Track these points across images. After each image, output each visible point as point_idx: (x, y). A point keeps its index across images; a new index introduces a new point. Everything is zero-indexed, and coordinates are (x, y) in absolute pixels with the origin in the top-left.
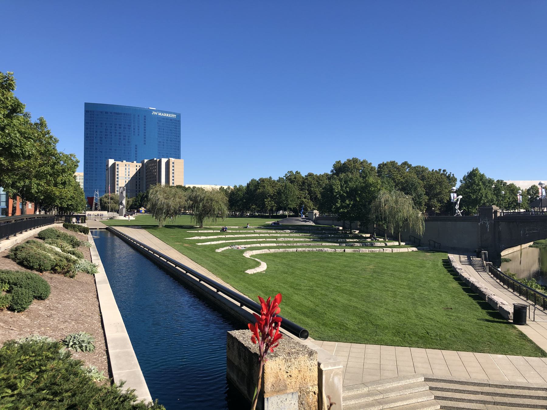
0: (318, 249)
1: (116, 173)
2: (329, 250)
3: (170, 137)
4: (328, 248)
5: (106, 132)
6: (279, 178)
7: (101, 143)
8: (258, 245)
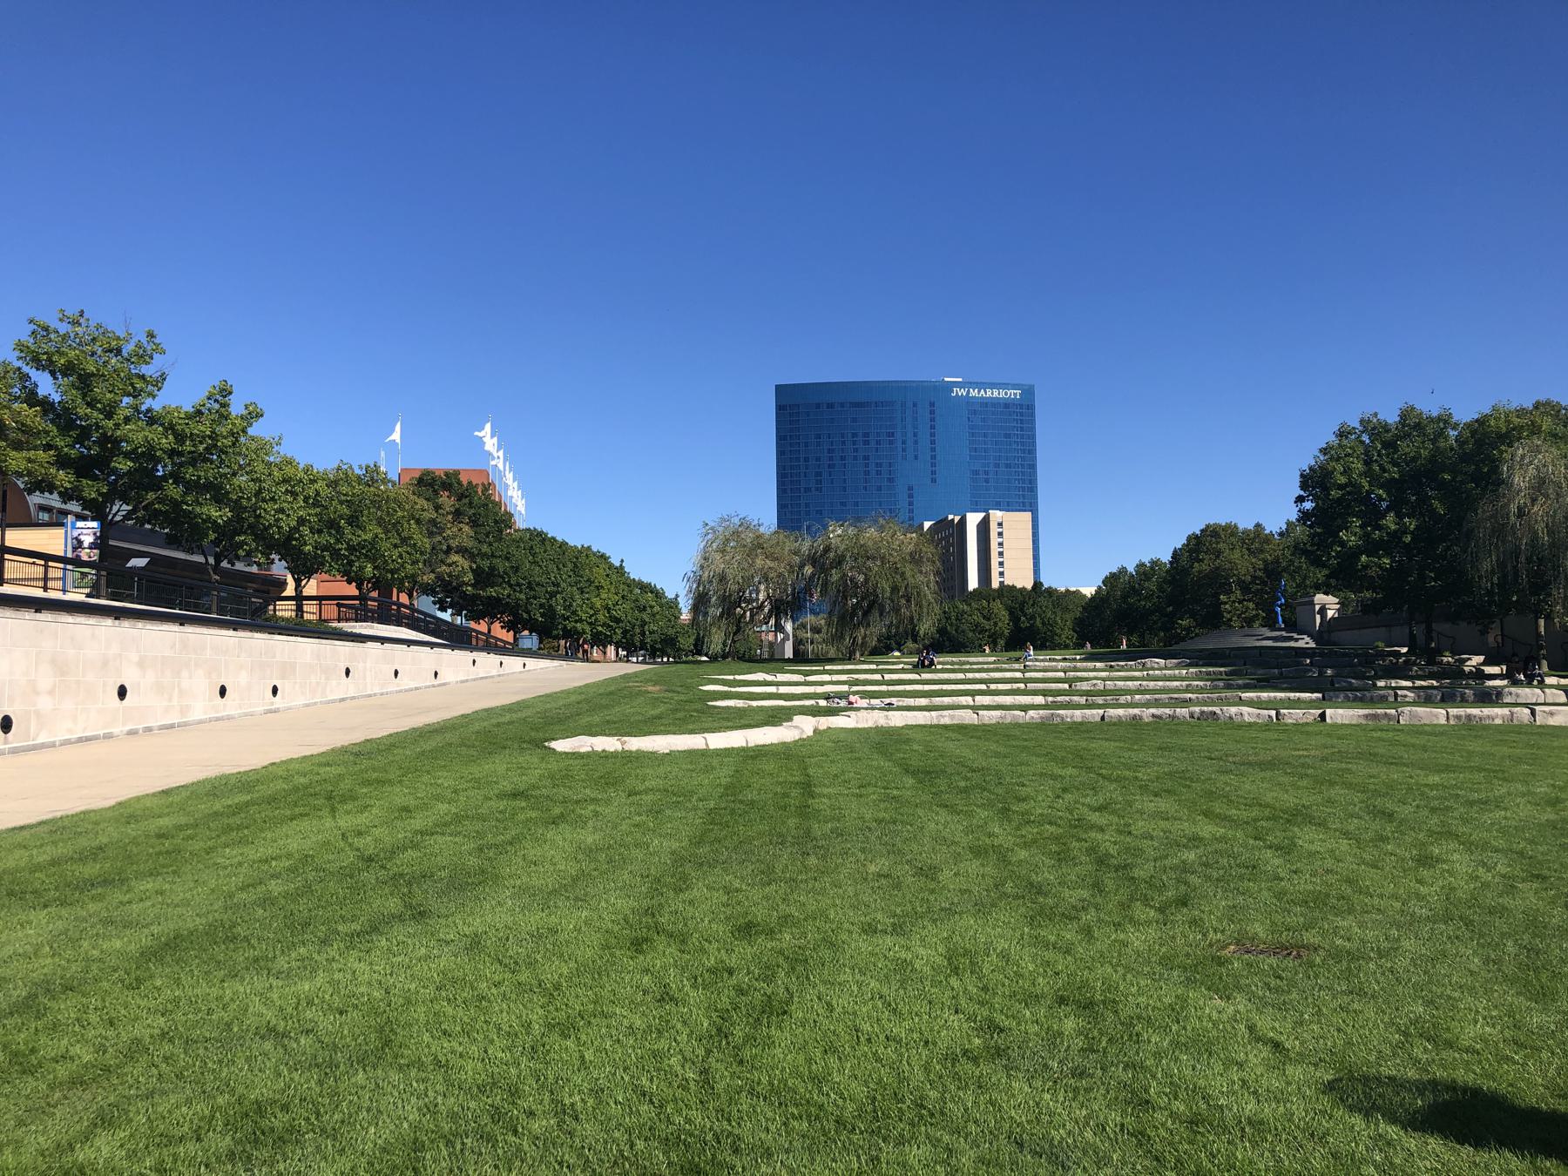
0: (1197, 709)
5: (831, 459)
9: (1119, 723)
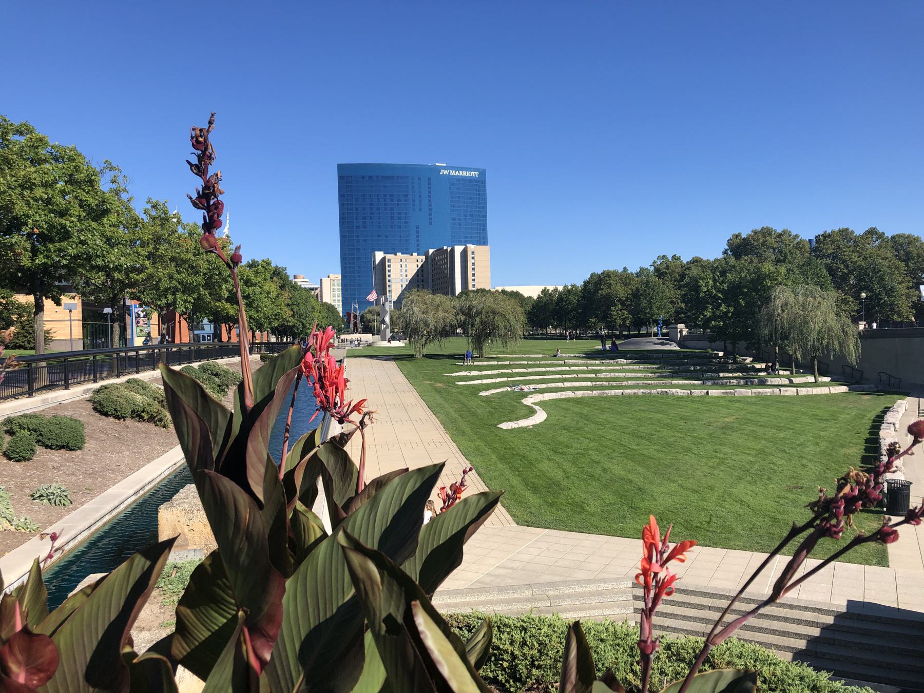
0: (660, 390)
1: (387, 274)
2: (680, 392)
3: (469, 211)
4: (679, 388)
6: (641, 269)
7: (365, 227)
8: (560, 385)
9: (629, 396)
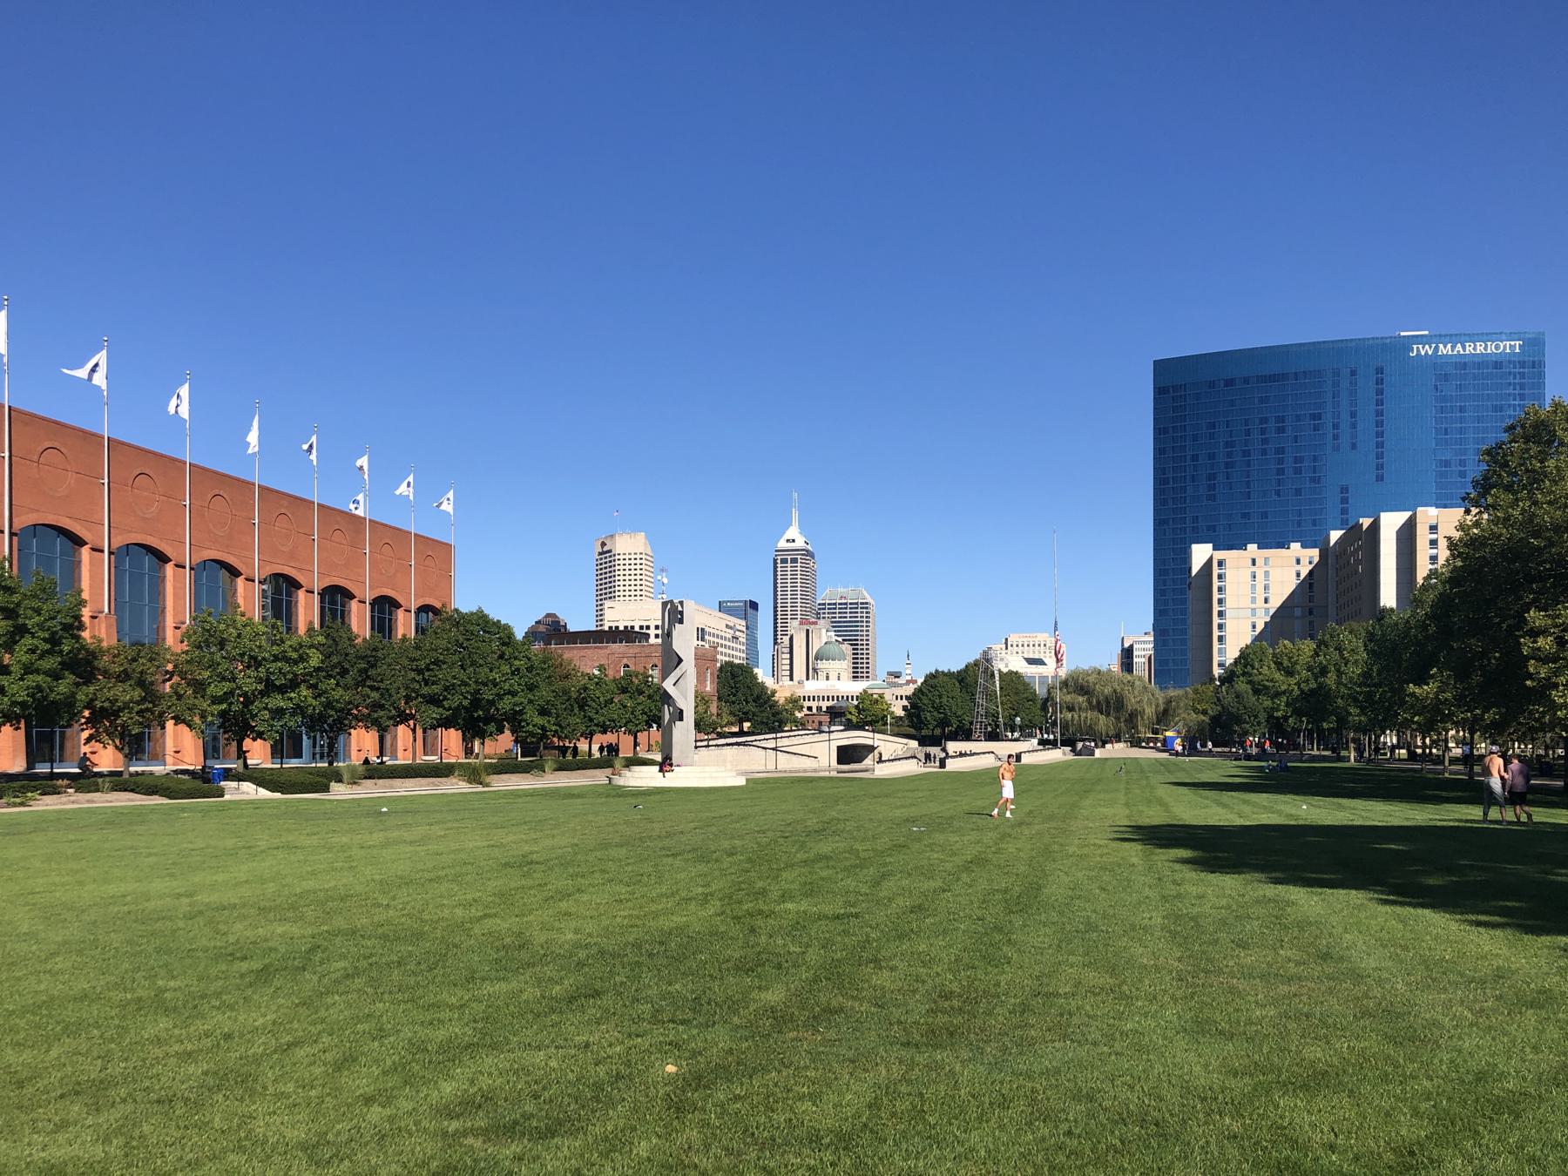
7: (1212, 498)
